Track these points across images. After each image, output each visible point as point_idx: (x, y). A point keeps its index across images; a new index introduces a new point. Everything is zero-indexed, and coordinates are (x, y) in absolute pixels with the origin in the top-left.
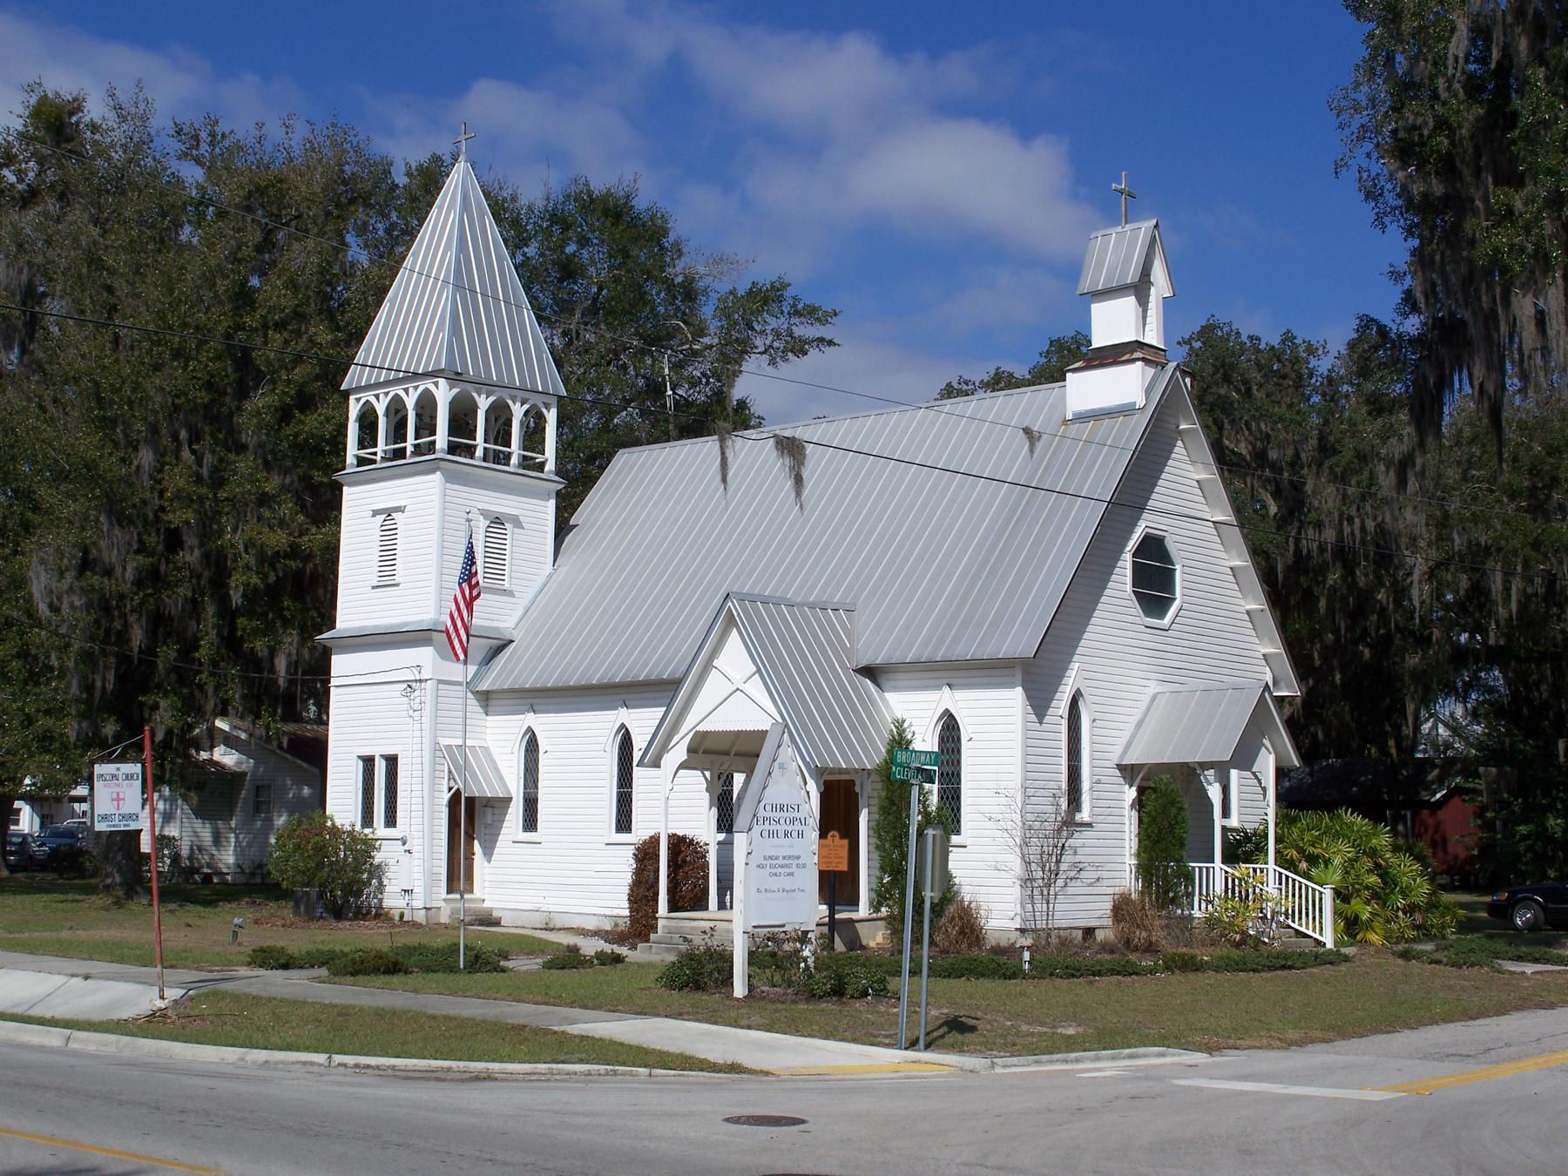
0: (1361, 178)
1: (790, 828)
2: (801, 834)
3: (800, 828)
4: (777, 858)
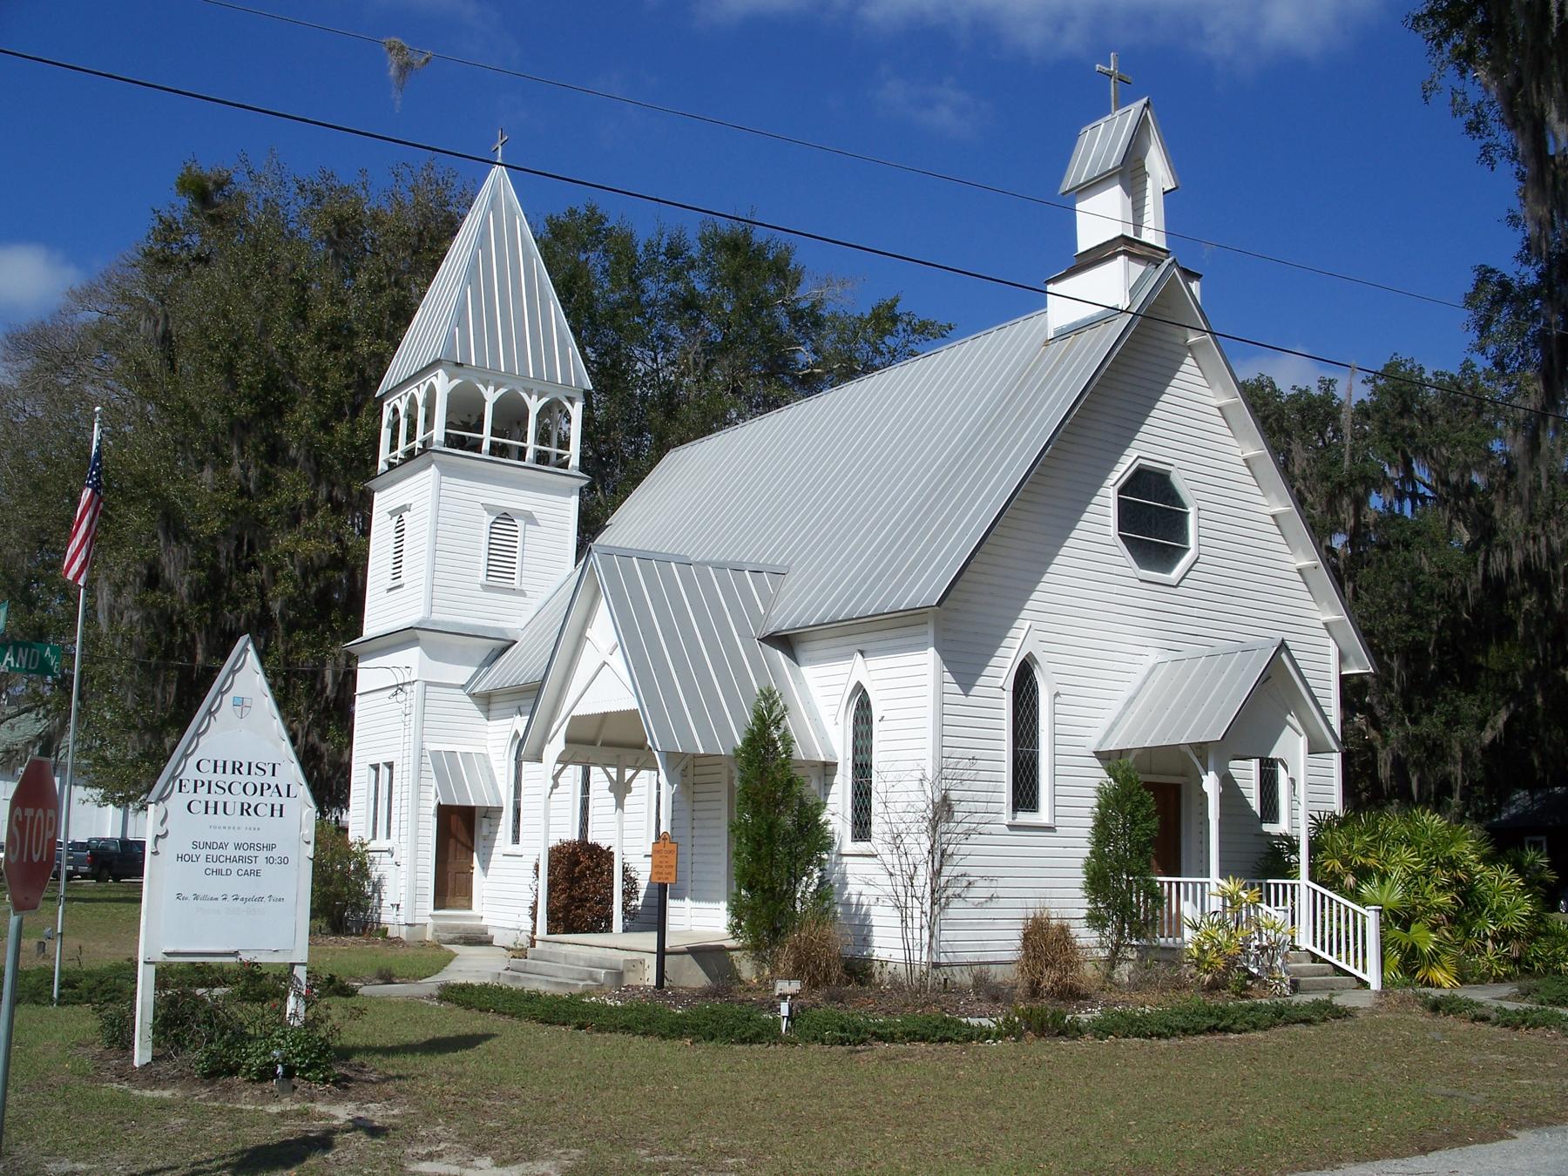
0: (1454, 100)
1: (254, 800)
2: (277, 811)
3: (277, 801)
4: (222, 846)
